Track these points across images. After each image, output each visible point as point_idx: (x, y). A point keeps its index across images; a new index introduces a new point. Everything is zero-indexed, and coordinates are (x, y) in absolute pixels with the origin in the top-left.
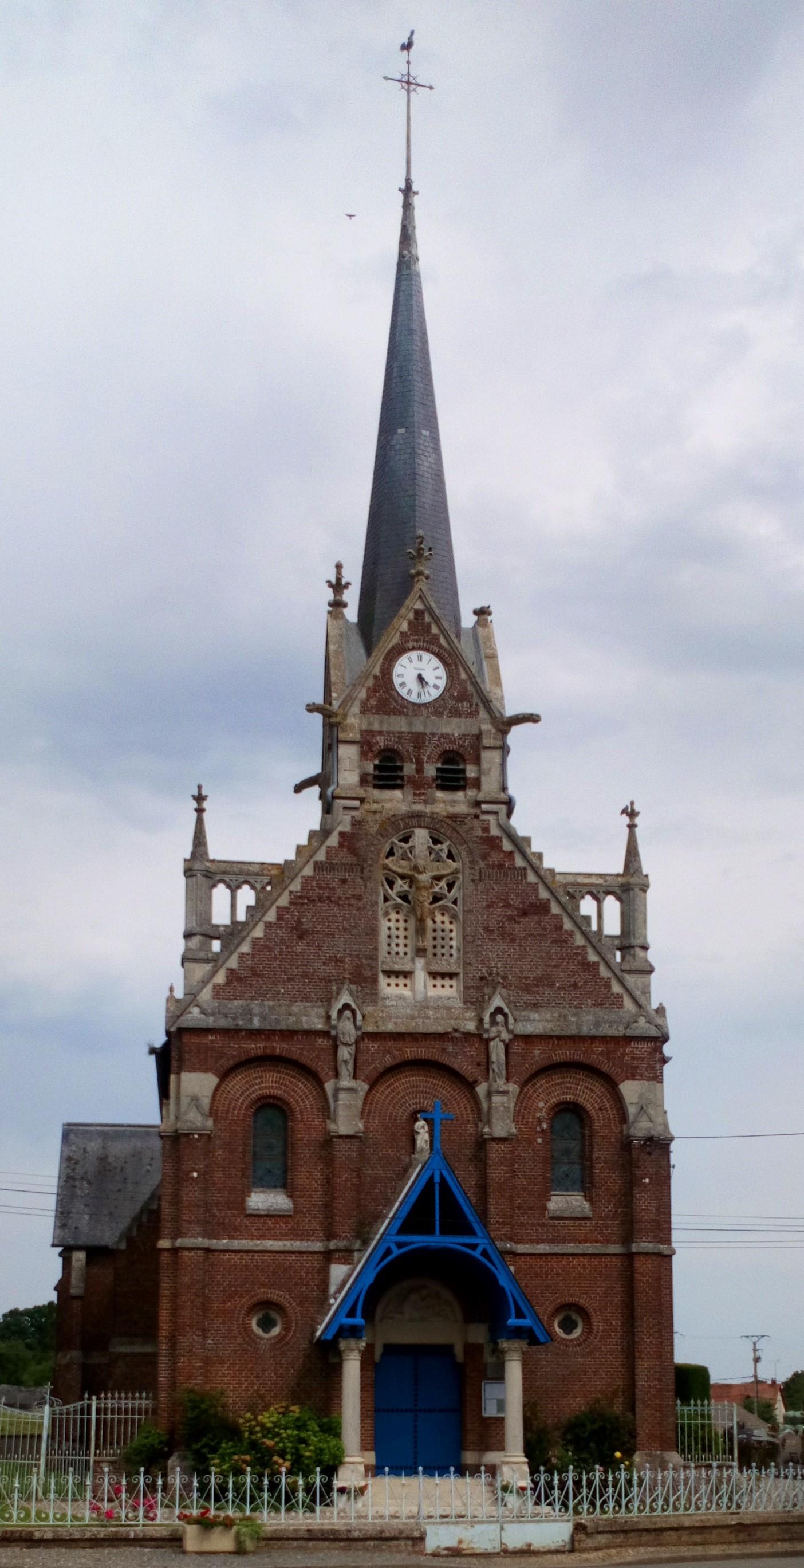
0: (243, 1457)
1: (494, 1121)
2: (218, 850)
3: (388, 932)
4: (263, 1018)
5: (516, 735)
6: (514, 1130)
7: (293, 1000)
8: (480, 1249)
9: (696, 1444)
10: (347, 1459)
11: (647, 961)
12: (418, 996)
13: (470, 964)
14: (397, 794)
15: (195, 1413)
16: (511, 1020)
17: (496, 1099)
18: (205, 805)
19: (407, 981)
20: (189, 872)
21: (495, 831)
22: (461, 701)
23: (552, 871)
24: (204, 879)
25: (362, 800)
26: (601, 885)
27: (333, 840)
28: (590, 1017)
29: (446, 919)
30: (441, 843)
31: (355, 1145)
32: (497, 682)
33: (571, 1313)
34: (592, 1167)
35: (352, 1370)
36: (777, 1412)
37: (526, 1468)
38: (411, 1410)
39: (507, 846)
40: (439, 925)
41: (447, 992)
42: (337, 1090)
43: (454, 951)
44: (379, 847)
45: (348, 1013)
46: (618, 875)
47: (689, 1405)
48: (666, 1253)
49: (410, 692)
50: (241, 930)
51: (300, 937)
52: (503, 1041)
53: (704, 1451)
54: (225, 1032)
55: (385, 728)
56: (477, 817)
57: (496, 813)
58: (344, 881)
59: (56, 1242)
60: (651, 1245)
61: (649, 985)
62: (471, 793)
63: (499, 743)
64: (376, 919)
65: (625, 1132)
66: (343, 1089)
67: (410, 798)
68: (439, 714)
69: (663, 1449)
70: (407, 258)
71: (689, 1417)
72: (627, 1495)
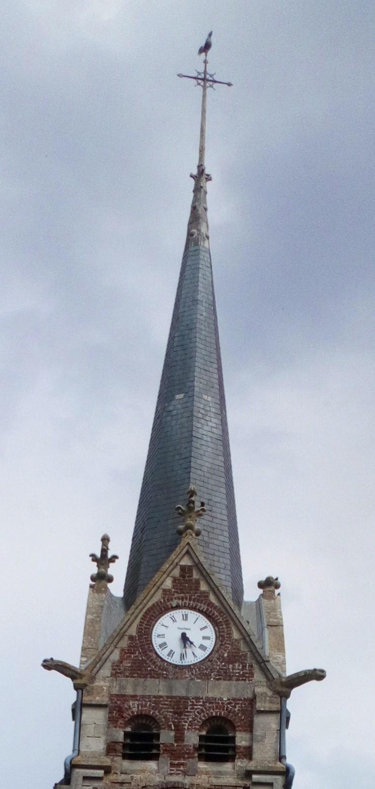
14: (152, 765)
22: (233, 663)
25: (108, 770)
49: (171, 653)
55: (139, 693)
62: (241, 764)
63: (275, 707)
67: (167, 768)
68: (206, 677)
70: (195, 235)
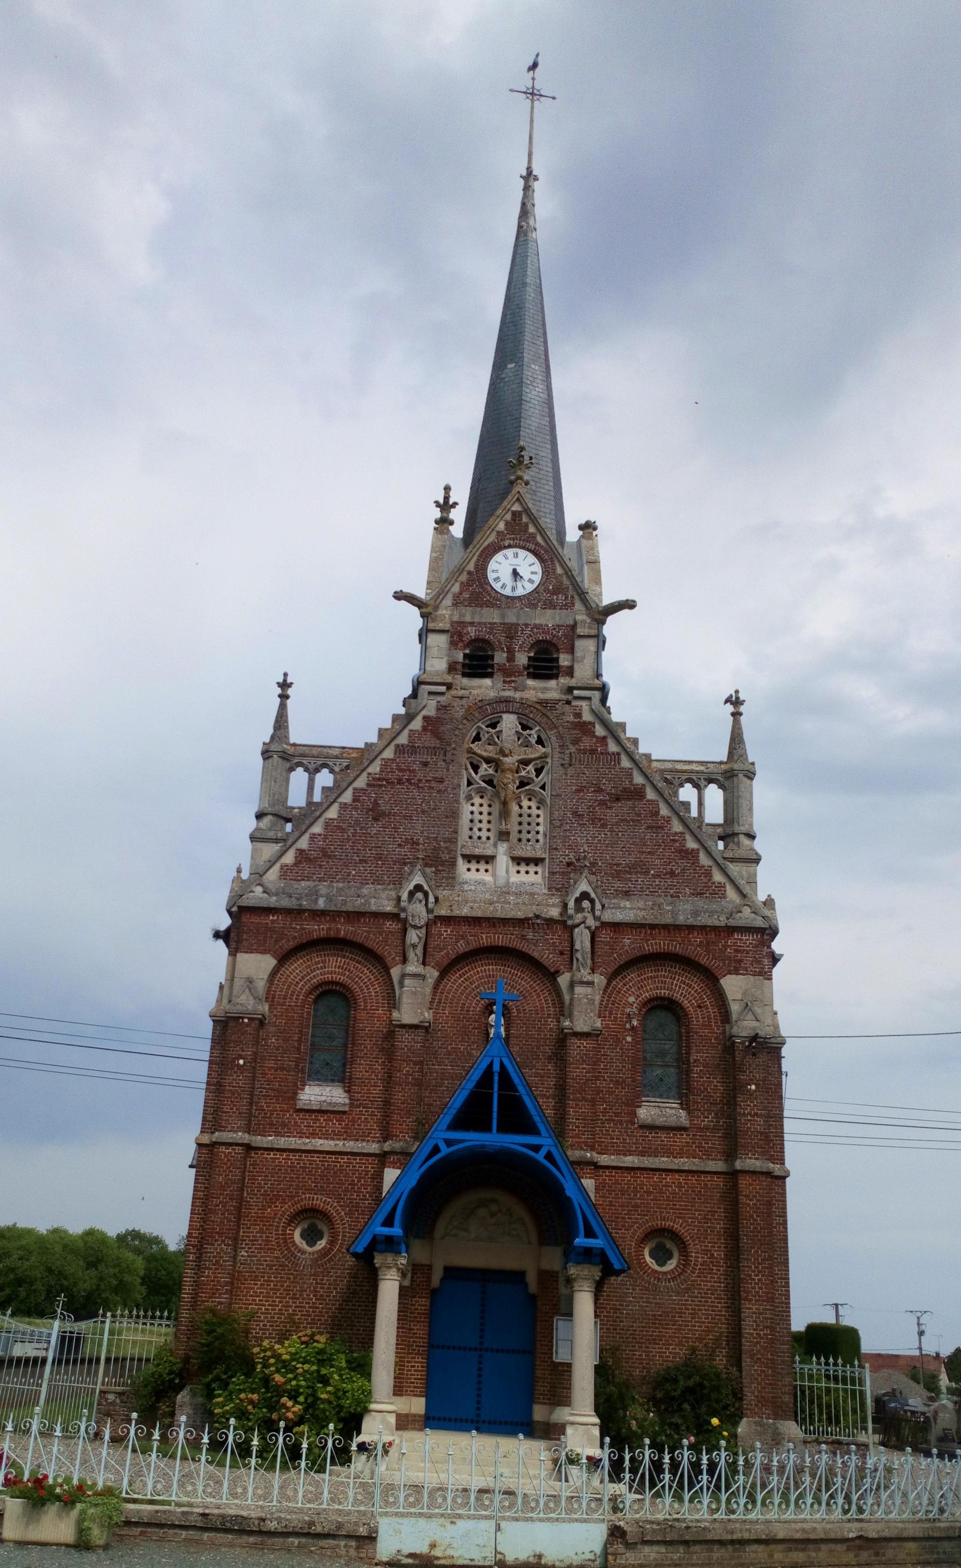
0: (250, 1396)
1: (576, 1013)
2: (298, 734)
3: (470, 816)
4: (329, 899)
5: (613, 626)
6: (598, 1024)
7: (364, 883)
8: (543, 1151)
9: (821, 1414)
10: (373, 1406)
11: (753, 849)
12: (498, 882)
13: (556, 849)
14: (487, 682)
15: (210, 1338)
16: (598, 906)
17: (579, 990)
18: (290, 692)
19: (489, 867)
20: (266, 754)
21: (587, 717)
22: (557, 594)
23: (648, 757)
24: (280, 760)
25: (449, 686)
26: (702, 772)
27: (417, 724)
28: (688, 907)
29: (533, 804)
30: (531, 729)
31: (419, 1036)
32: (597, 580)
33: (664, 1240)
34: (689, 1072)
35: (389, 1292)
36: (941, 1383)
37: (596, 1432)
38: (476, 1349)
39: (599, 731)
40: (525, 810)
41: (532, 878)
42: (403, 976)
43: (540, 837)
44: (464, 731)
45: (420, 895)
46: (721, 763)
47: (811, 1363)
48: (778, 1173)
49: (504, 586)
50: (315, 811)
51: (376, 819)
52: (588, 928)
53: (830, 1422)
54: (287, 912)
55: (477, 620)
56: (568, 702)
57: (589, 699)
58: (425, 764)
59: (195, 1163)
60: (758, 1163)
61: (755, 875)
62: (564, 681)
63: (593, 632)
64: (457, 802)
65: (728, 1033)
66: (409, 975)
67: (500, 685)
68: (533, 606)
69: (776, 1416)
71: (136, 1330)
72: (691, 1485)
